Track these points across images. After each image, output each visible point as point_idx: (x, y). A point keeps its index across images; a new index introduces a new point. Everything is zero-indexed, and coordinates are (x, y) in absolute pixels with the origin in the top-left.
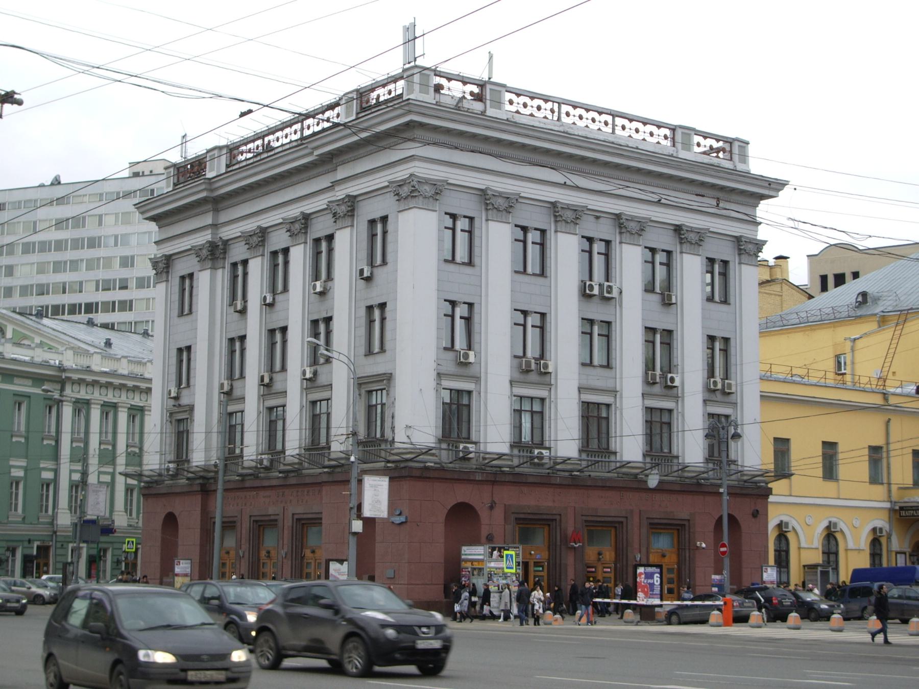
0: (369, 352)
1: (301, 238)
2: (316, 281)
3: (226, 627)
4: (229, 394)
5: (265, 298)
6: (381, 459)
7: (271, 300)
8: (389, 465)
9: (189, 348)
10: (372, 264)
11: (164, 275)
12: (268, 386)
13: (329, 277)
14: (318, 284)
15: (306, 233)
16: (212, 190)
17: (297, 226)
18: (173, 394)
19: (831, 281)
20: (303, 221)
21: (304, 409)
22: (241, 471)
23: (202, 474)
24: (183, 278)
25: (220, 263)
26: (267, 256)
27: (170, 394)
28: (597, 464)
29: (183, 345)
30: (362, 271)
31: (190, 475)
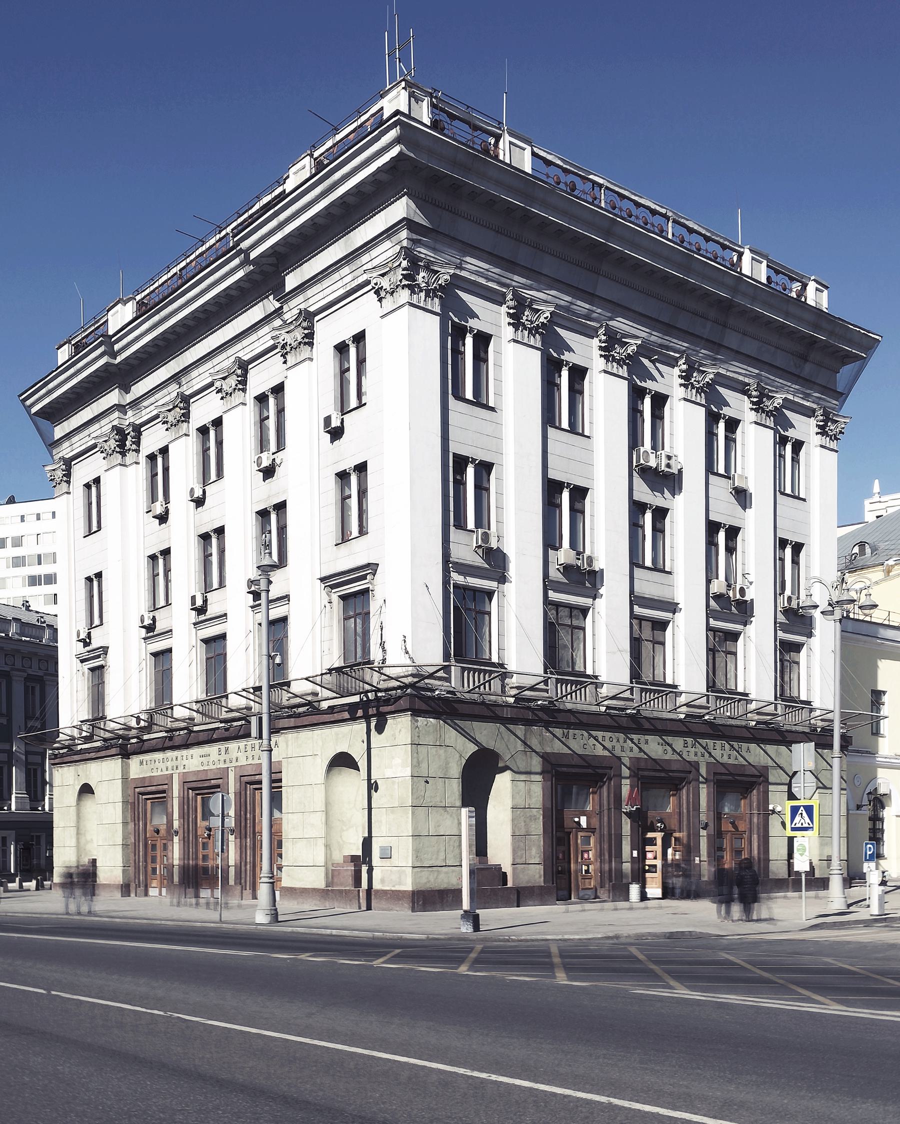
0: (344, 538)
1: (238, 397)
2: (261, 452)
3: (403, 288)
4: (150, 628)
5: (192, 490)
6: (161, 728)
7: (201, 493)
8: (380, 694)
9: (99, 575)
10: (344, 410)
11: (64, 485)
12: (201, 610)
13: (281, 446)
14: (264, 455)
15: (244, 390)
16: (114, 355)
17: (232, 381)
18: (82, 636)
19: (51, 797)
20: (239, 372)
21: (251, 648)
22: (224, 715)
23: (121, 732)
24: (88, 486)
25: (130, 457)
26: (193, 433)
27: (78, 636)
28: (471, 687)
29: (91, 573)
30: (328, 420)
31: (108, 735)
